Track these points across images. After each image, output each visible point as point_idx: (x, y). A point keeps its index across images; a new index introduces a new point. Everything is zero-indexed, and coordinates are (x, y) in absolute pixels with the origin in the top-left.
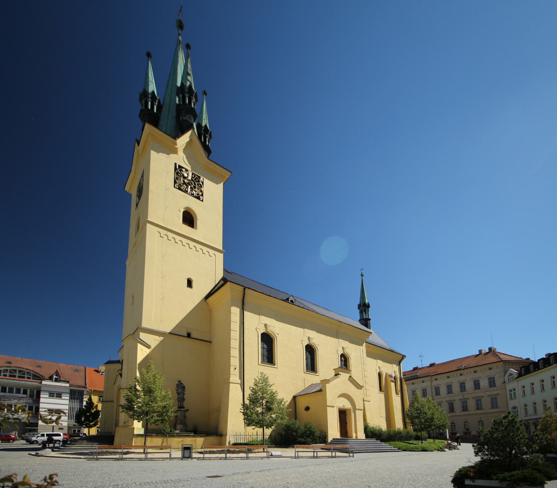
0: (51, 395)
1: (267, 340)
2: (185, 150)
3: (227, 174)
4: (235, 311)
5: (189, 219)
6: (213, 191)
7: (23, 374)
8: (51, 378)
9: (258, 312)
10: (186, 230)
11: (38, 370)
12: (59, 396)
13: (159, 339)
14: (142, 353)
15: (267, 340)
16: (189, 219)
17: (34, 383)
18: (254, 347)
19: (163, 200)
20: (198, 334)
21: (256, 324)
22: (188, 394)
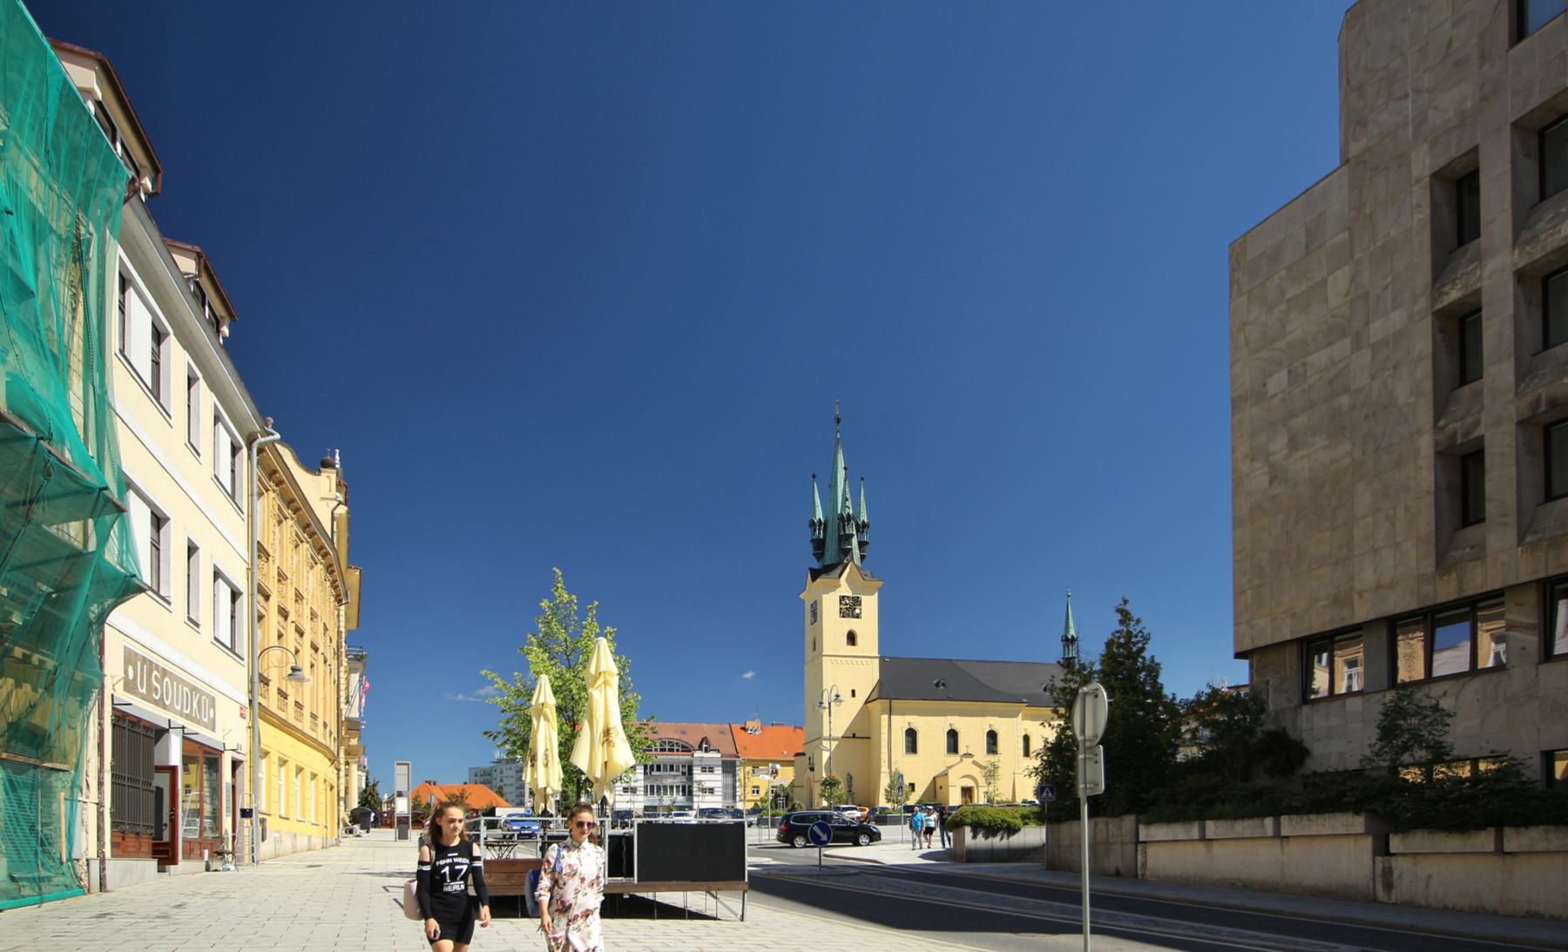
0: (704, 770)
1: (911, 734)
2: (847, 580)
3: (880, 584)
4: (885, 718)
5: (851, 638)
6: (870, 604)
7: (669, 746)
8: (700, 748)
9: (903, 713)
10: (851, 650)
11: (683, 738)
12: (711, 770)
13: (834, 744)
14: (826, 755)
15: (911, 734)
16: (851, 638)
17: (685, 757)
18: (900, 740)
19: (833, 626)
20: (861, 736)
21: (901, 723)
22: (854, 783)
